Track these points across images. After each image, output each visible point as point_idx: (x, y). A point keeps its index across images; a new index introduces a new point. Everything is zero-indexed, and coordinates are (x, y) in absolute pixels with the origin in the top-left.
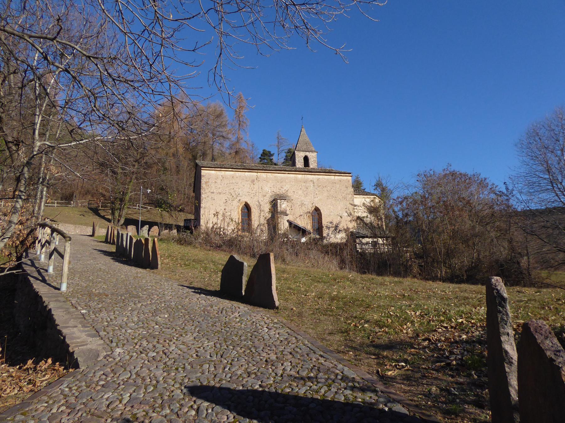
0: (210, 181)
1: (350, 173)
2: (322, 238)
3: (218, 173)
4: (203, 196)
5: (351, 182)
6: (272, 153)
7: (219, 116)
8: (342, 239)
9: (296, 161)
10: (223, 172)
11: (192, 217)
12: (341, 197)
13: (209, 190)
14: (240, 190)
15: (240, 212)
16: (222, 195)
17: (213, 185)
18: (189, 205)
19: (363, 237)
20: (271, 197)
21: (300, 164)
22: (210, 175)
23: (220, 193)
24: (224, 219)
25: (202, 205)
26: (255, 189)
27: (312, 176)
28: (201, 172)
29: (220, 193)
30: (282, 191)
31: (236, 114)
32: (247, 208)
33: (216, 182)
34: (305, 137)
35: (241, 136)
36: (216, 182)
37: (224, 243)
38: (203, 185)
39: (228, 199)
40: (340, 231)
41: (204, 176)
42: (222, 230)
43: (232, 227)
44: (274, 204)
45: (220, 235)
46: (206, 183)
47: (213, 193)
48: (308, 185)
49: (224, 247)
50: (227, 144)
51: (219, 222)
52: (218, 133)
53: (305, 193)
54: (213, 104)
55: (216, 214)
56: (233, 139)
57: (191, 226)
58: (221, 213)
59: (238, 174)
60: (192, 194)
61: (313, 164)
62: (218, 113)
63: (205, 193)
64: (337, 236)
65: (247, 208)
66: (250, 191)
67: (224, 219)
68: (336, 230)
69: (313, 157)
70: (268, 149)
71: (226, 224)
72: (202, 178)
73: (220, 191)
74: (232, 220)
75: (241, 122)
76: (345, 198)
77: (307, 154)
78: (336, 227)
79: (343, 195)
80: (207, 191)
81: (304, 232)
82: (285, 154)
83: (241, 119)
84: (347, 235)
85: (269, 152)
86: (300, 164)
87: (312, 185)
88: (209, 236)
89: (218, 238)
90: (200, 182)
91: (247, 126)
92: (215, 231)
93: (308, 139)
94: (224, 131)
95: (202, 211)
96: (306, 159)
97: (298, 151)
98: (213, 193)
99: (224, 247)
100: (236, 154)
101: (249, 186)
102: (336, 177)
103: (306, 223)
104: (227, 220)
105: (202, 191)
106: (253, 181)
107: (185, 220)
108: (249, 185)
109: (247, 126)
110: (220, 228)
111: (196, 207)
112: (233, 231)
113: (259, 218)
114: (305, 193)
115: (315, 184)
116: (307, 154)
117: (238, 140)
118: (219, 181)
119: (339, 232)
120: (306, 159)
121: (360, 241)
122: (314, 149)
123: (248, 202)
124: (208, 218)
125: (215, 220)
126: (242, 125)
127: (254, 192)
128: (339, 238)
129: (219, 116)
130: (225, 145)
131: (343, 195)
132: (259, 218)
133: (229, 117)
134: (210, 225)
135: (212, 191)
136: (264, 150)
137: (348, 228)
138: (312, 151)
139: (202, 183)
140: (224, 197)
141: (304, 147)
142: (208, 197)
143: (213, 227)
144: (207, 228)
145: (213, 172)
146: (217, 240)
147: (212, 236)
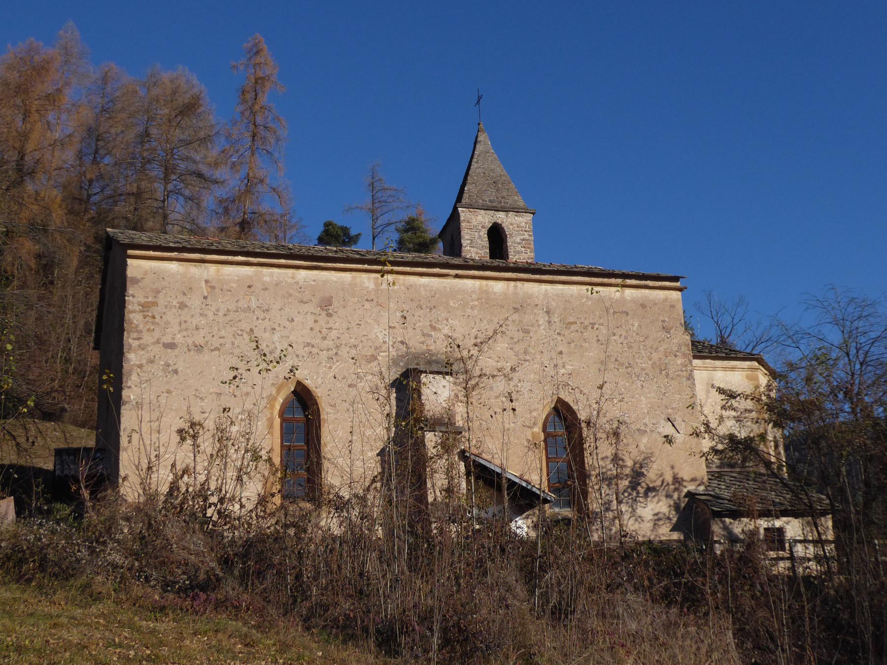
0: (161, 301)
1: (675, 279)
2: (585, 516)
3: (195, 270)
4: (132, 358)
5: (680, 307)
6: (353, 233)
7: (190, 108)
8: (657, 519)
9: (465, 242)
10: (213, 268)
11: (86, 438)
12: (647, 365)
13: (157, 334)
14: (276, 337)
15: (277, 421)
16: (206, 356)
17: (171, 317)
18: (80, 397)
19: (735, 515)
20: (395, 362)
21: (474, 246)
22: (160, 275)
23: (199, 348)
24: (221, 454)
25: (129, 394)
26: (334, 334)
27: (544, 287)
28: (124, 266)
29: (199, 348)
30: (438, 346)
31: (244, 101)
32: (303, 411)
33: (182, 306)
34: (488, 161)
35: (260, 174)
36: (182, 306)
37: (226, 562)
38: (134, 316)
39: (242, 366)
40: (649, 489)
41: (136, 281)
42: (214, 499)
43: (252, 490)
44: (405, 386)
45: (207, 520)
46: (145, 307)
47: (171, 346)
48: (528, 318)
49: (230, 588)
50: (209, 200)
51: (202, 464)
52: (182, 165)
53: (520, 348)
54: (166, 76)
55: (189, 432)
56: (233, 182)
57: (80, 479)
58: (210, 424)
59: (270, 275)
60: (93, 358)
61: (520, 251)
62: (184, 99)
63: (142, 347)
64: (640, 511)
65: (303, 411)
66: (317, 341)
67: (221, 454)
68: (634, 485)
69: (519, 228)
70: (339, 221)
71: (231, 473)
72: (131, 290)
73: (200, 341)
74: (256, 458)
75: (261, 131)
76: (662, 369)
77: (500, 217)
78: (637, 475)
79: (655, 356)
80: (147, 338)
81: (524, 499)
82: (396, 236)
83: (259, 120)
84: (677, 507)
85: (345, 230)
86: (474, 246)
87: (542, 320)
88: (157, 533)
89: (197, 542)
90: (122, 304)
91: (278, 140)
92: (184, 506)
93: (499, 169)
94: (203, 157)
95: (128, 419)
96: (497, 237)
97: (469, 206)
98: (171, 346)
99: (230, 588)
100: (243, 229)
101: (311, 323)
102: (628, 292)
103: (527, 467)
104: (235, 456)
105: (129, 339)
106: (326, 304)
107: (59, 453)
108: (310, 318)
109: (278, 140)
110: (203, 493)
111: (103, 396)
112: (263, 501)
113: (353, 449)
114: (520, 348)
115: (555, 318)
116: (500, 217)
117: (250, 184)
118: (195, 302)
119: (646, 495)
120: (497, 237)
121: (726, 528)
122: (521, 203)
123: (308, 383)
124: (153, 449)
125: (184, 455)
126: (264, 139)
127: (329, 343)
128: (649, 520)
129: (190, 108)
130: (204, 204)
131: (655, 356)
132: (353, 449)
133: (218, 113)
134: (162, 479)
135: (167, 339)
136: (327, 225)
137: (678, 481)
138: (517, 210)
139: (129, 307)
140: (218, 366)
141: (490, 196)
142: (151, 361)
143: (174, 487)
144: (151, 498)
145: (173, 266)
146: (192, 549)
147: (172, 530)
